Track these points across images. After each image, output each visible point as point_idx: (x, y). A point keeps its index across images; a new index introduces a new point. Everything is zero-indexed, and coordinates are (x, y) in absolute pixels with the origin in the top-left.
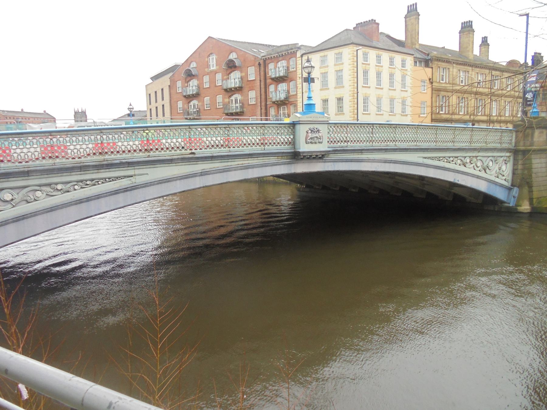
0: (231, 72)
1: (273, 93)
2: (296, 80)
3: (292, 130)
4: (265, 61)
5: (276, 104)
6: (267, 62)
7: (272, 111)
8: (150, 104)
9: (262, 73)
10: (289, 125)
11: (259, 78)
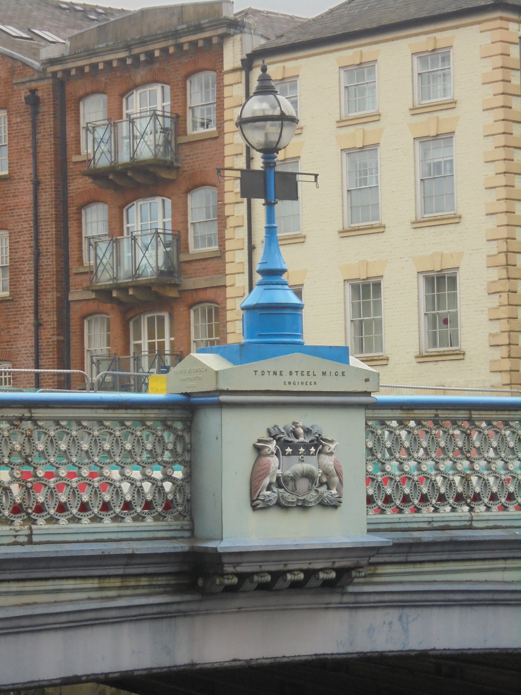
1: (103, 246)
2: (217, 185)
3: (179, 438)
4: (61, 83)
5: (117, 301)
6: (74, 88)
7: (96, 340)
9: (47, 146)
10: (163, 413)
11: (29, 171)
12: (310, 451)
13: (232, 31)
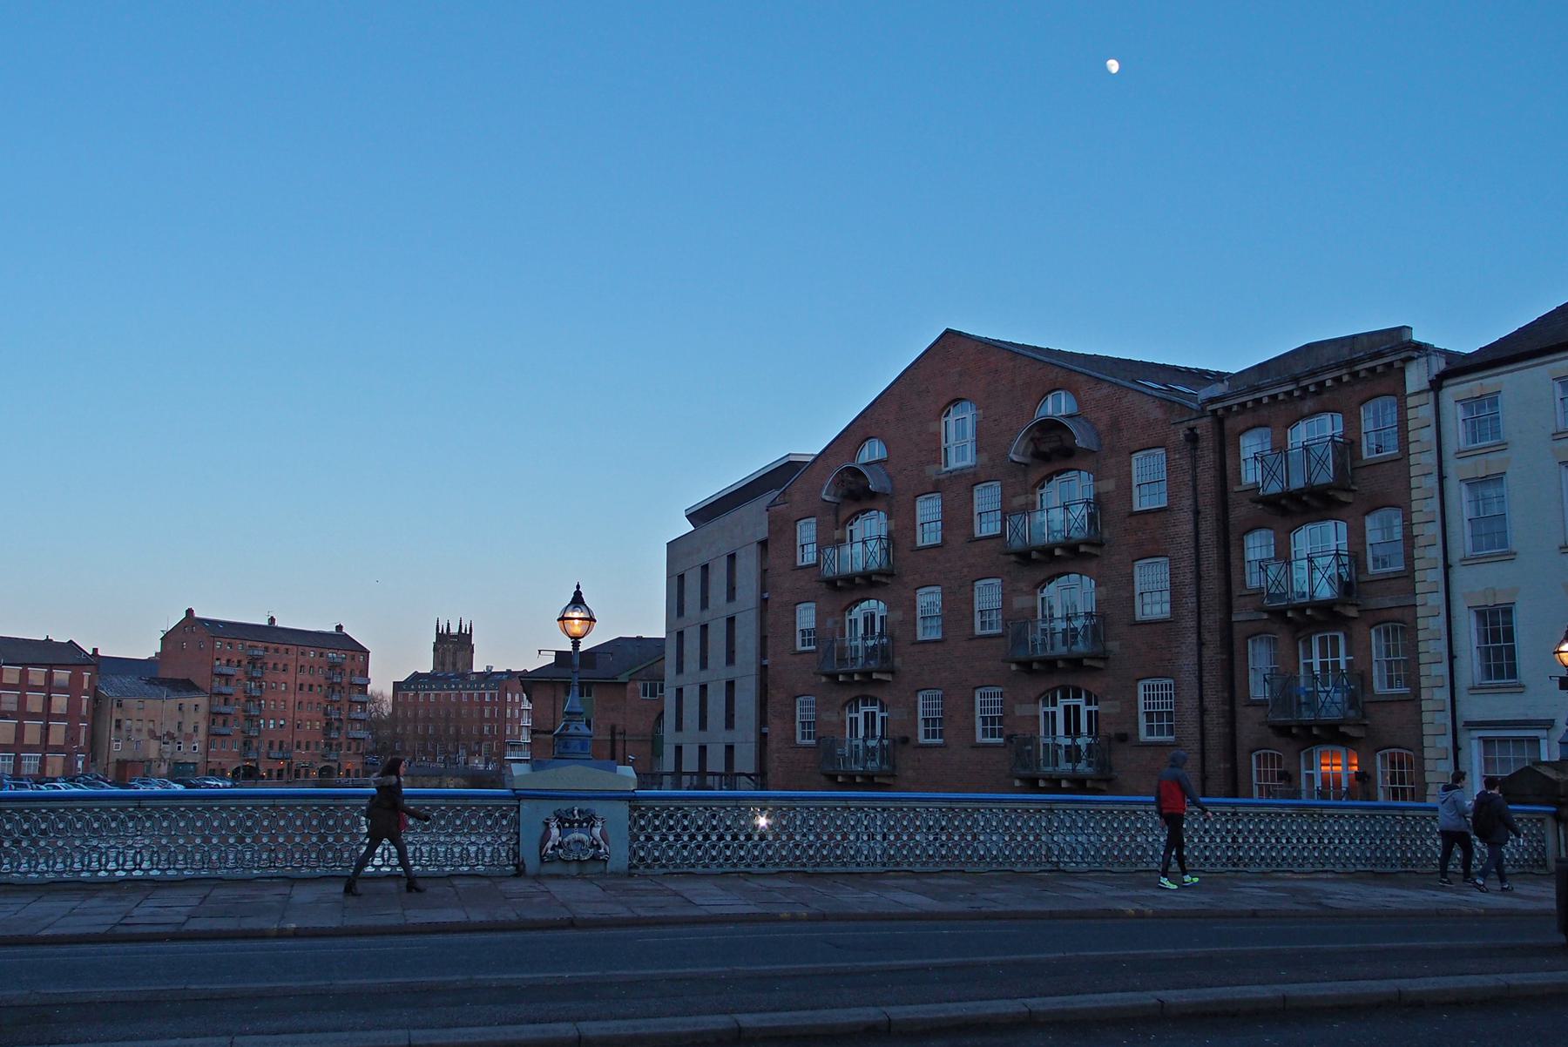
4: (1219, 420)
8: (681, 612)
9: (1207, 478)
11: (1187, 503)
13: (1416, 354)
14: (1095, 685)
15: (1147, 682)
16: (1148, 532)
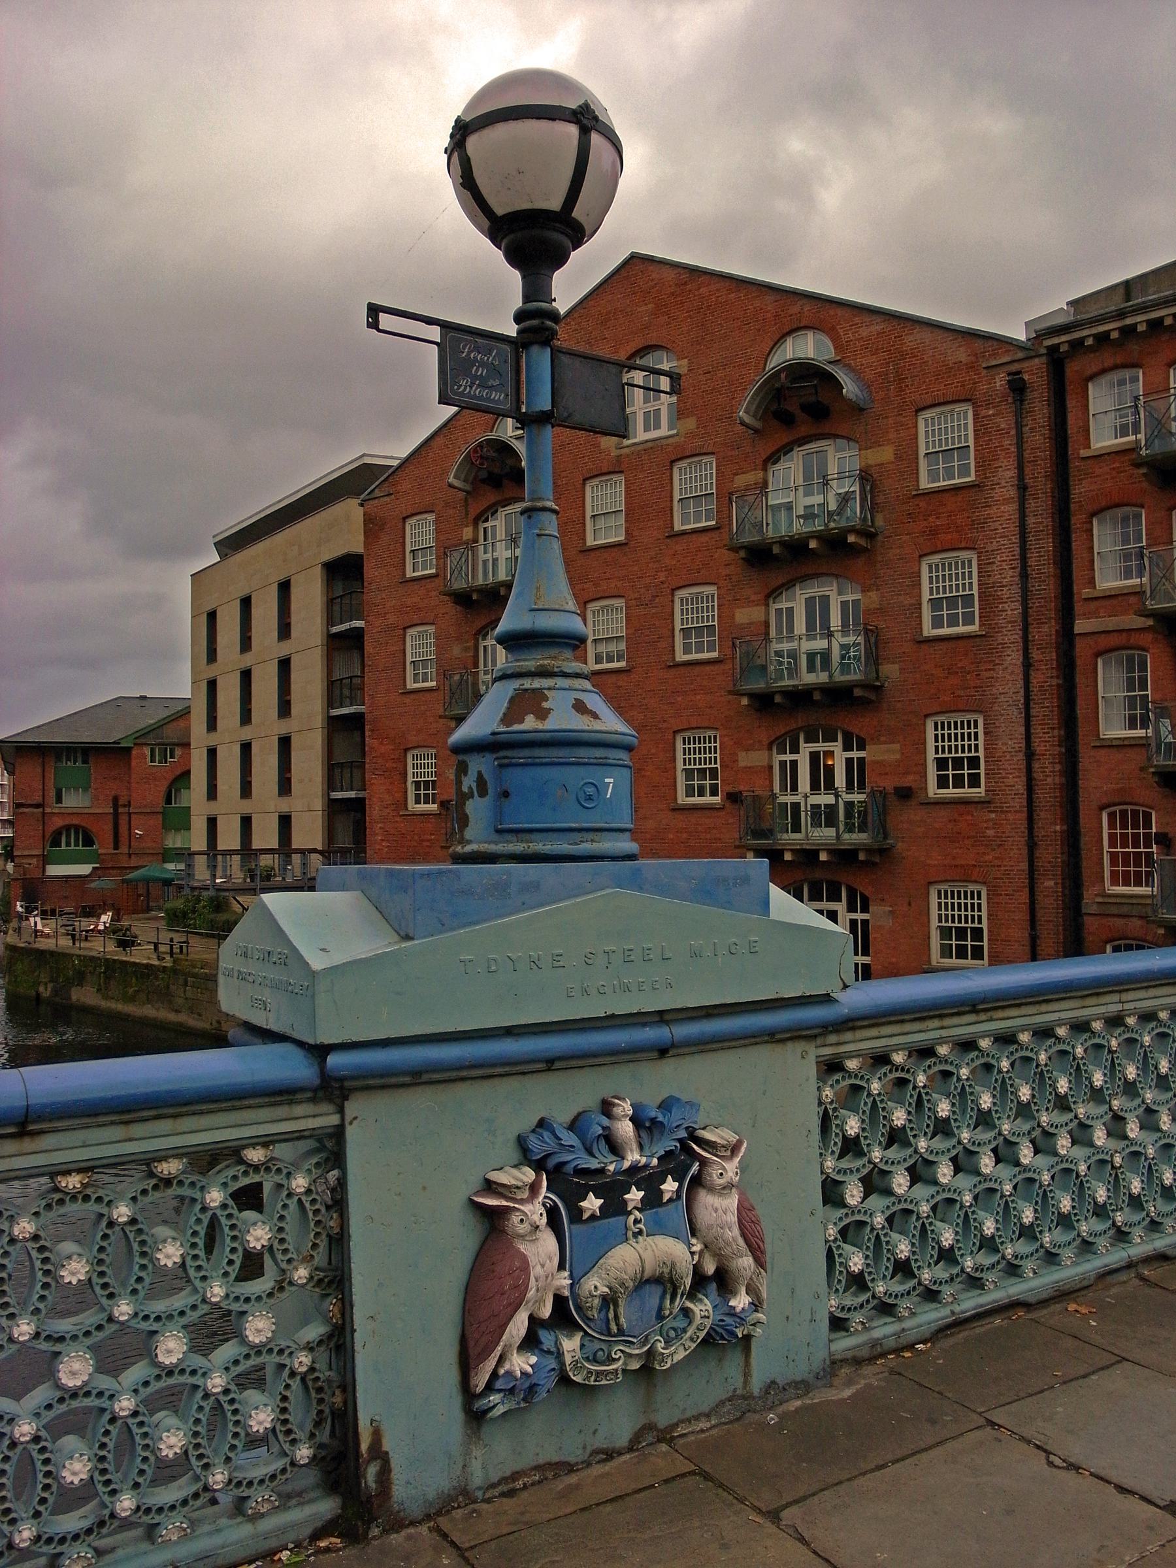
0: (786, 449)
4: (1057, 362)
8: (212, 656)
9: (1039, 438)
11: (1007, 473)
12: (661, 1192)
14: (860, 725)
15: (940, 719)
16: (947, 519)
